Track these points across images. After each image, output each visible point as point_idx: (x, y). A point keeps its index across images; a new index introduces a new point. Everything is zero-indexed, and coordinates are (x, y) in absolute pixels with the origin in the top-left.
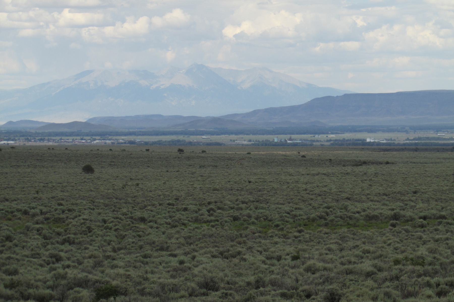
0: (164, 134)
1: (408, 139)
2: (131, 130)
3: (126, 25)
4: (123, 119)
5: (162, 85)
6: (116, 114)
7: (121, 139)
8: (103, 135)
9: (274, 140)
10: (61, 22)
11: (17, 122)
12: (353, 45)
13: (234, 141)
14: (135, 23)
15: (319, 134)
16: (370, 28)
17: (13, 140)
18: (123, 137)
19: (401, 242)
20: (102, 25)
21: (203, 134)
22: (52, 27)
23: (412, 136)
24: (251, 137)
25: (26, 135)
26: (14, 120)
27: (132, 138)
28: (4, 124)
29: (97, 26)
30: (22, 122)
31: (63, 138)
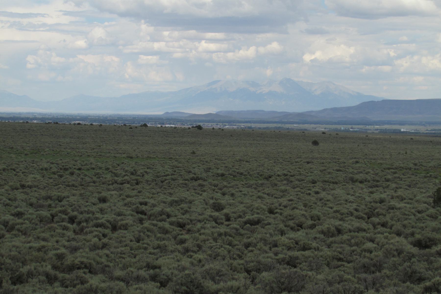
0: (268, 122)
1: (427, 130)
2: (247, 120)
3: (241, 52)
4: (239, 113)
5: (264, 91)
6: (234, 109)
7: (242, 125)
8: (230, 122)
9: (341, 128)
10: (200, 49)
12: (387, 68)
13: (315, 128)
14: (247, 50)
15: (369, 125)
16: (399, 57)
18: (243, 124)
20: (226, 51)
21: (293, 124)
22: (194, 52)
23: (430, 128)
29: (223, 52)
30: (174, 112)
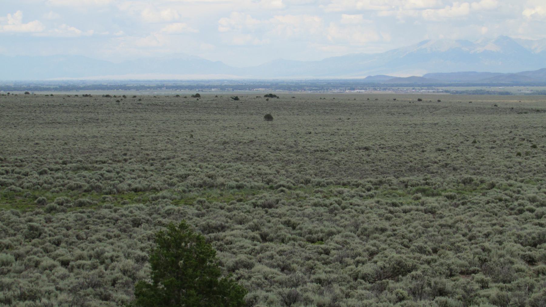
7: (440, 89)
8: (430, 86)
11: (375, 76)
13: (520, 91)
17: (364, 89)
19: (261, 240)
24: (531, 88)
25: (375, 86)
26: (372, 75)
27: (178, 92)
28: (366, 78)
30: (378, 76)
31: (400, 88)
